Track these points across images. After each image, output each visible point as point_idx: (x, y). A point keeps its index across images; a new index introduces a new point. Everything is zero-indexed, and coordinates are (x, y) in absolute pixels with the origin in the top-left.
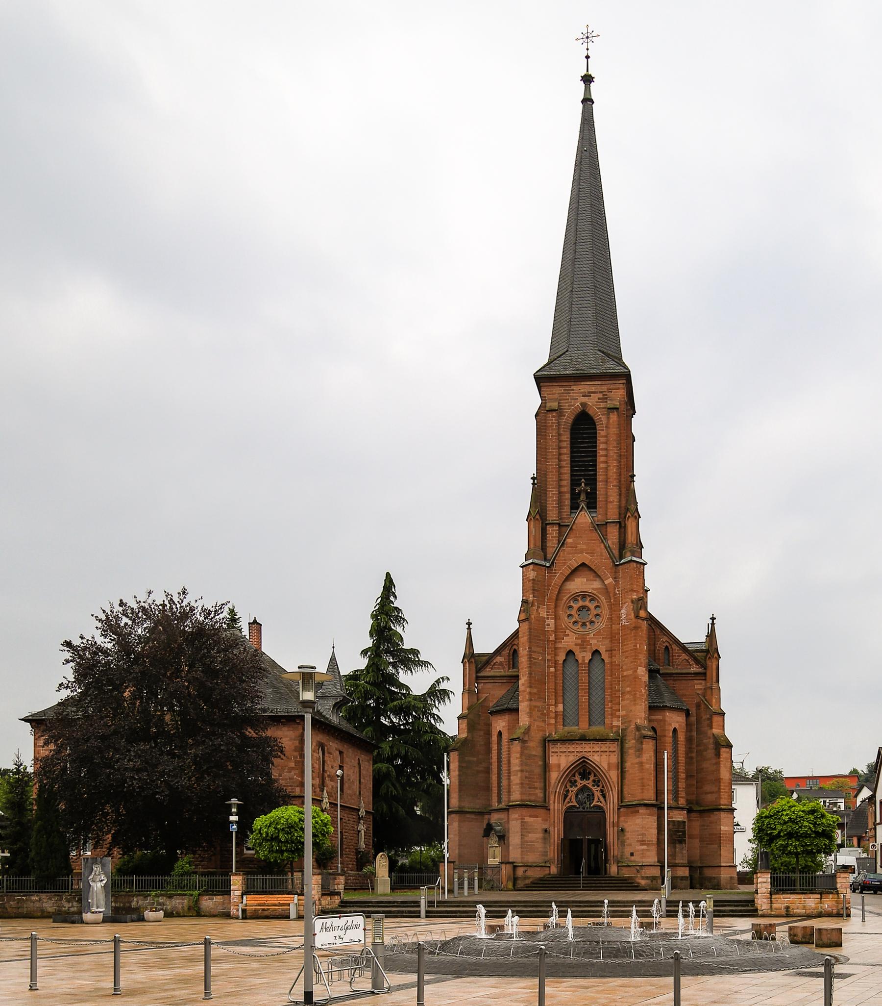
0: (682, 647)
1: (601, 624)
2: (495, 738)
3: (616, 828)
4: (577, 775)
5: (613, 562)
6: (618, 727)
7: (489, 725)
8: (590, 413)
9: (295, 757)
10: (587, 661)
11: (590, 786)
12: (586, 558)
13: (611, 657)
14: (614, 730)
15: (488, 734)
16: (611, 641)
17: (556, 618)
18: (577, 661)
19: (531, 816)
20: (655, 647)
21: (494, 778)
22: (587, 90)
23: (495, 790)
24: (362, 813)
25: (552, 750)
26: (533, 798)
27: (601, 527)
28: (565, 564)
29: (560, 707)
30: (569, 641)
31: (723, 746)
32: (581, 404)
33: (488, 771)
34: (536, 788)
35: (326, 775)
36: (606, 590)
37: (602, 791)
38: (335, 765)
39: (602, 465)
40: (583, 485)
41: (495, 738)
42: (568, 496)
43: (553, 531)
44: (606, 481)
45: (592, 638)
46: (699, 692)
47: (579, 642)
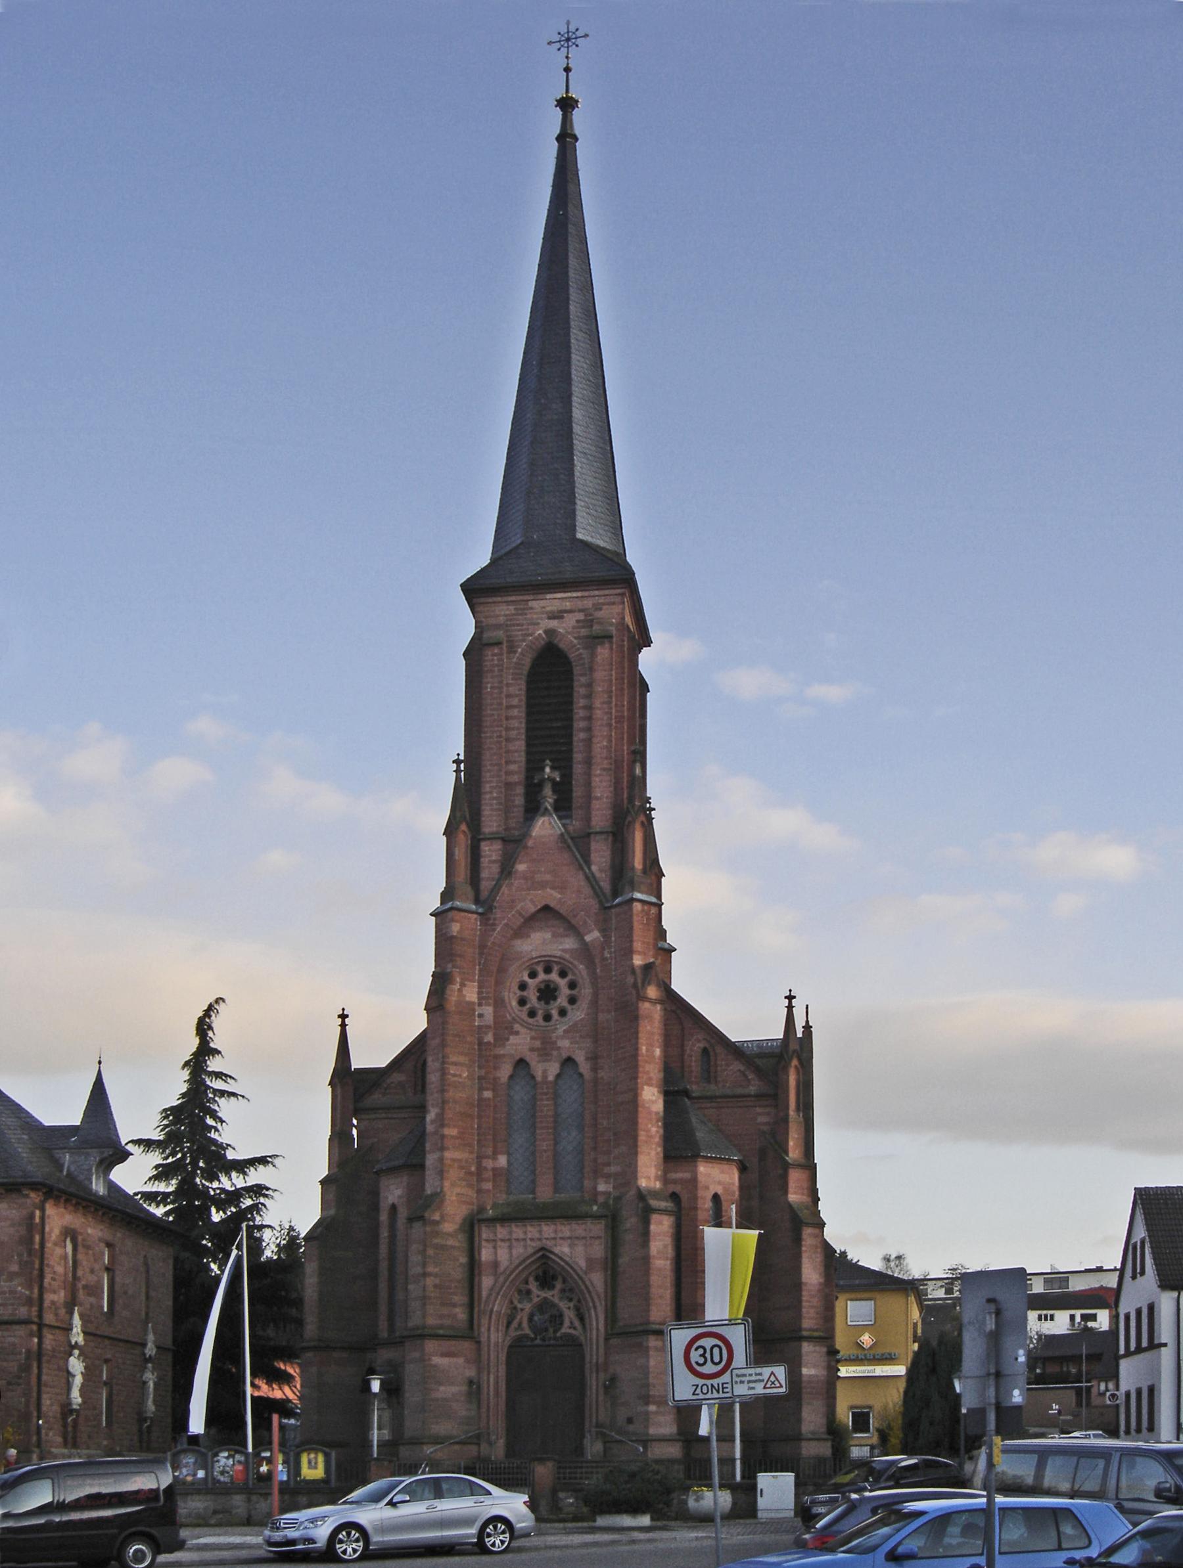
0: (736, 1050)
1: (578, 1014)
2: (384, 1217)
3: (602, 1376)
4: (531, 1279)
5: (601, 902)
6: (607, 1194)
7: (375, 1194)
8: (562, 646)
9: (20, 1255)
10: (551, 1078)
11: (556, 1300)
12: (552, 897)
13: (595, 1069)
14: (601, 1199)
15: (375, 1207)
16: (596, 1041)
17: (499, 1003)
18: (533, 1077)
19: (444, 1355)
20: (683, 1051)
21: (383, 1286)
22: (566, 121)
23: (383, 1308)
24: (150, 1350)
25: (484, 1236)
26: (447, 1322)
27: (577, 844)
28: (512, 908)
29: (502, 1161)
30: (520, 1043)
31: (808, 1225)
32: (546, 632)
33: (374, 1274)
34: (454, 1305)
35: (80, 1285)
36: (586, 952)
37: (577, 1309)
38: (97, 1267)
39: (582, 735)
40: (548, 770)
41: (384, 1217)
42: (520, 790)
43: (491, 852)
44: (588, 762)
45: (562, 1038)
46: (765, 1128)
47: (538, 1044)
